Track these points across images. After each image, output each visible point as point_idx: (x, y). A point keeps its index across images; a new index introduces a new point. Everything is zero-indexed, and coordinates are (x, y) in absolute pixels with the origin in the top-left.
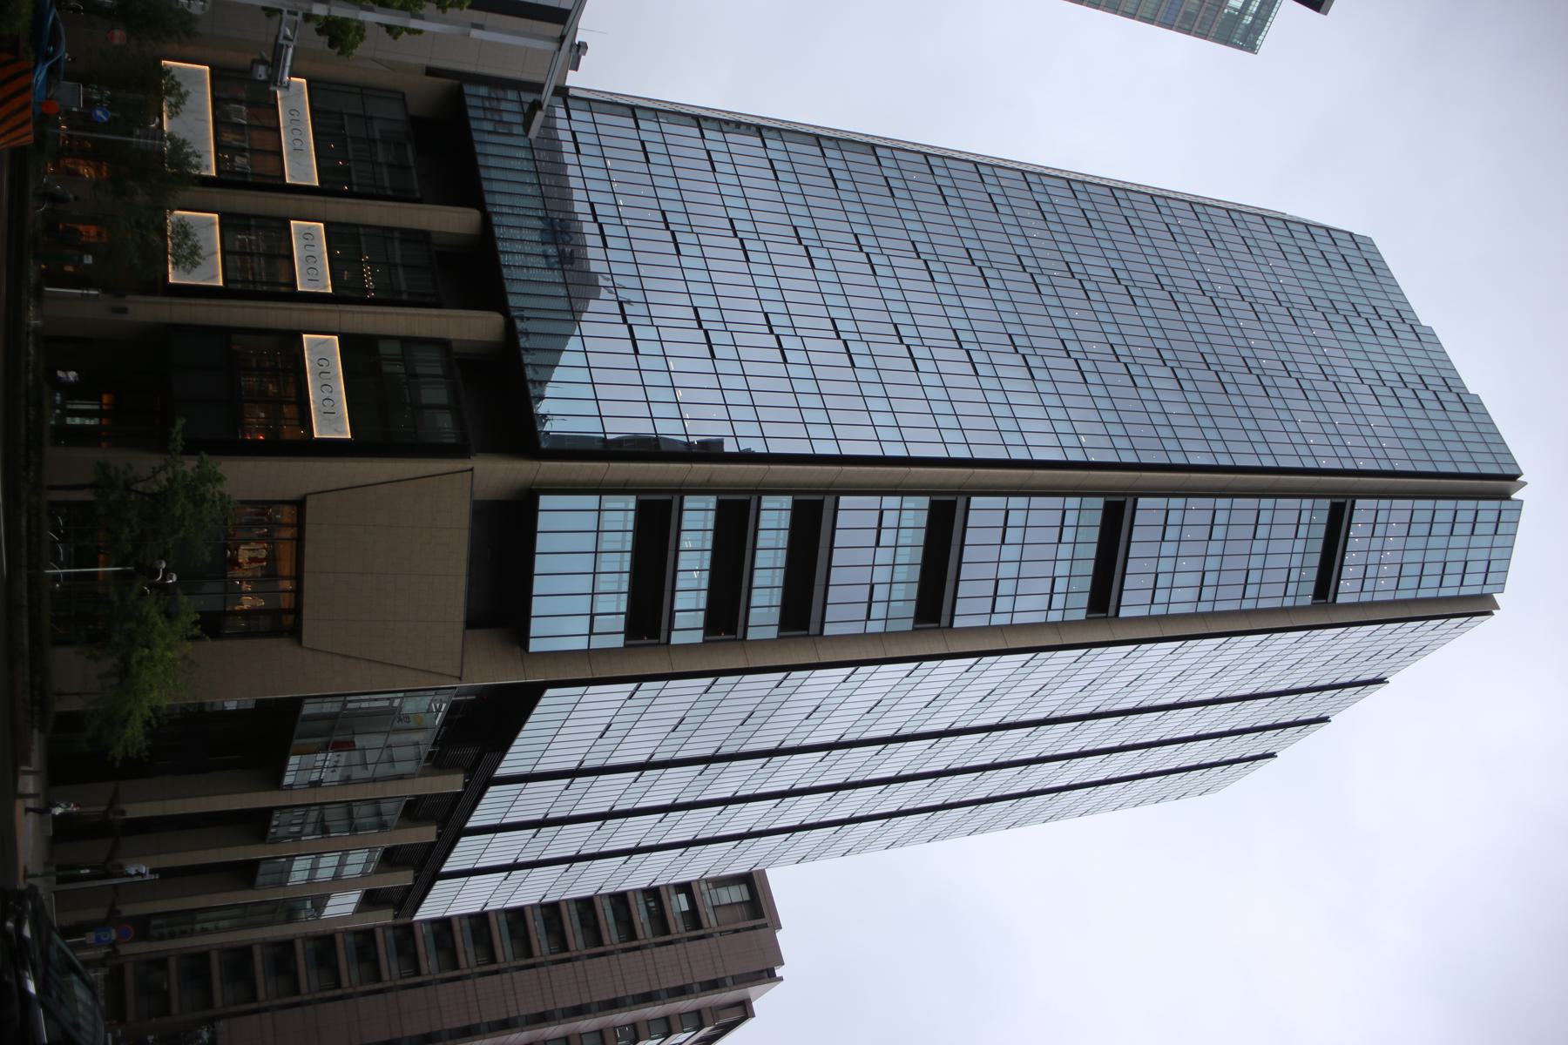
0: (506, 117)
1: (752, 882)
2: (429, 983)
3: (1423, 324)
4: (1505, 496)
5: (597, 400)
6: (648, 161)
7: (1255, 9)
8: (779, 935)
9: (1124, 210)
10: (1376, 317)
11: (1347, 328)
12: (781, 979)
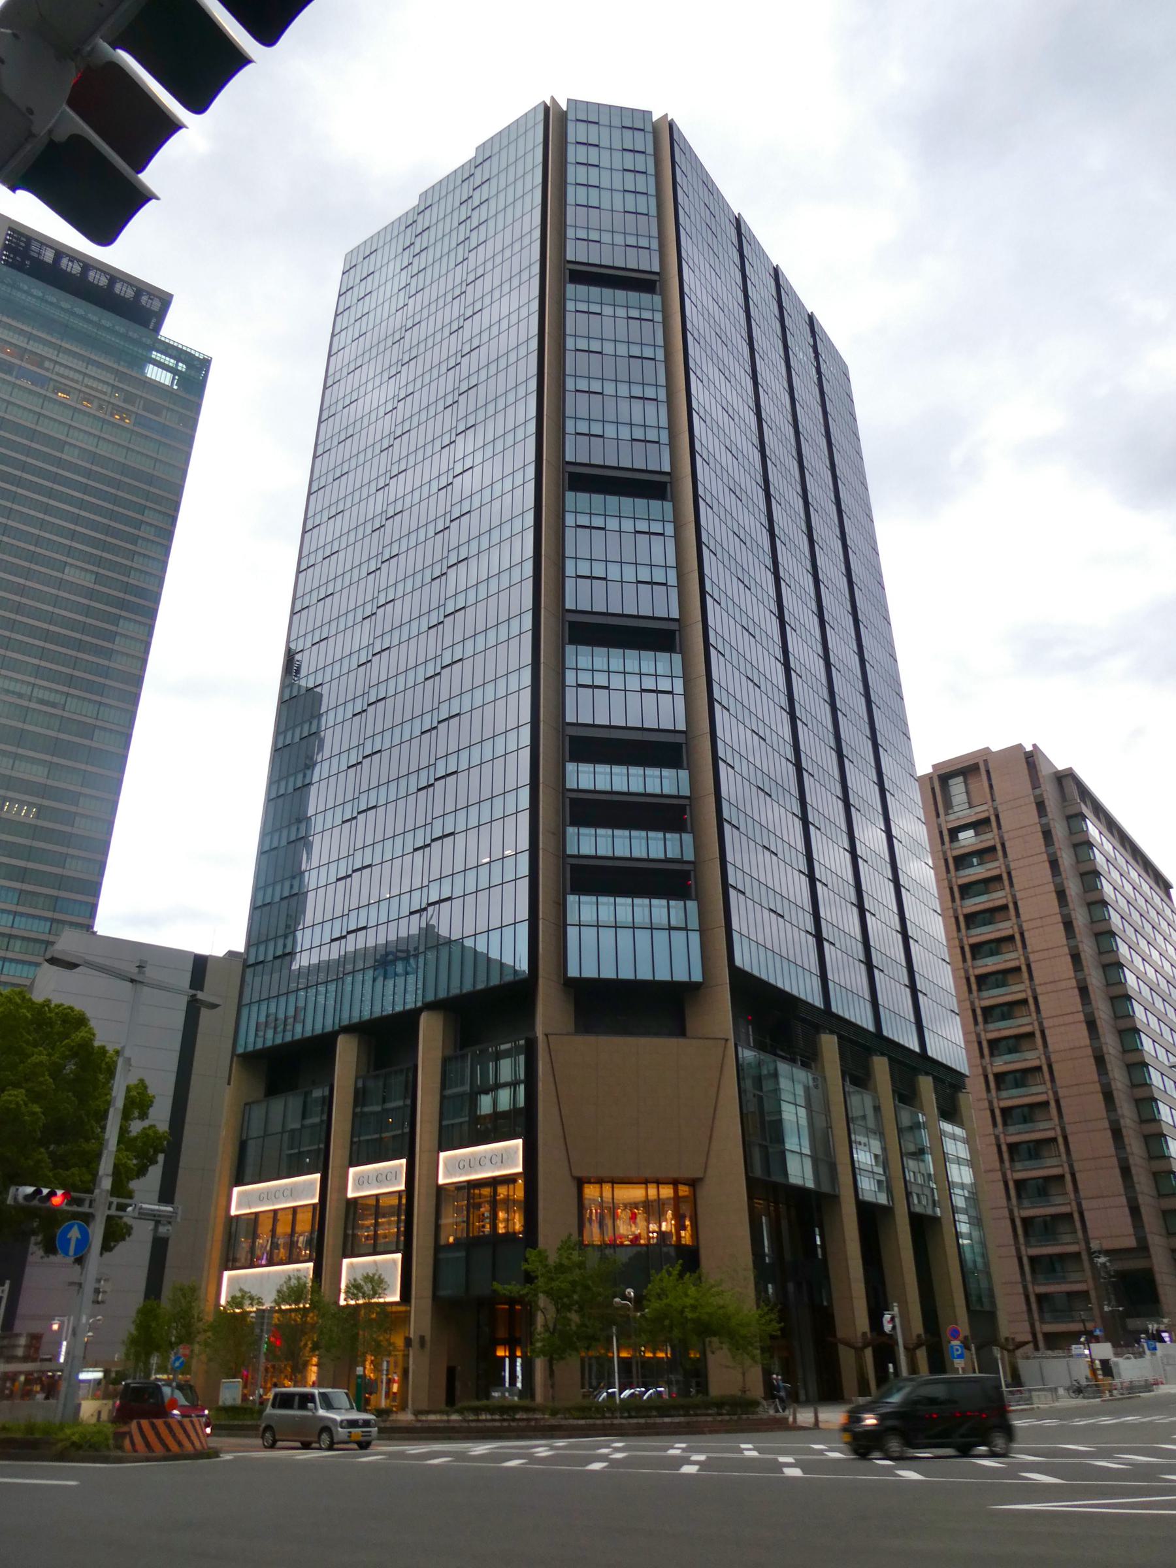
0: (291, 1012)
1: (944, 776)
2: (1048, 1058)
3: (416, 203)
4: (563, 117)
5: (488, 931)
6: (370, 866)
7: (172, 361)
8: (994, 749)
9: (328, 482)
10: (470, 201)
11: (483, 228)
12: (1035, 746)
